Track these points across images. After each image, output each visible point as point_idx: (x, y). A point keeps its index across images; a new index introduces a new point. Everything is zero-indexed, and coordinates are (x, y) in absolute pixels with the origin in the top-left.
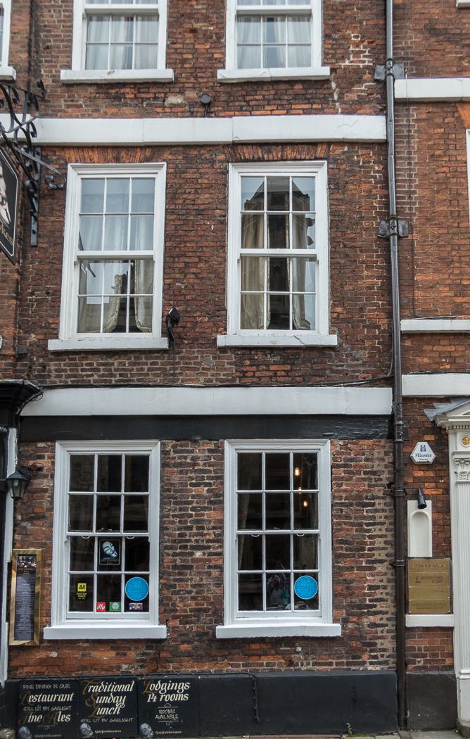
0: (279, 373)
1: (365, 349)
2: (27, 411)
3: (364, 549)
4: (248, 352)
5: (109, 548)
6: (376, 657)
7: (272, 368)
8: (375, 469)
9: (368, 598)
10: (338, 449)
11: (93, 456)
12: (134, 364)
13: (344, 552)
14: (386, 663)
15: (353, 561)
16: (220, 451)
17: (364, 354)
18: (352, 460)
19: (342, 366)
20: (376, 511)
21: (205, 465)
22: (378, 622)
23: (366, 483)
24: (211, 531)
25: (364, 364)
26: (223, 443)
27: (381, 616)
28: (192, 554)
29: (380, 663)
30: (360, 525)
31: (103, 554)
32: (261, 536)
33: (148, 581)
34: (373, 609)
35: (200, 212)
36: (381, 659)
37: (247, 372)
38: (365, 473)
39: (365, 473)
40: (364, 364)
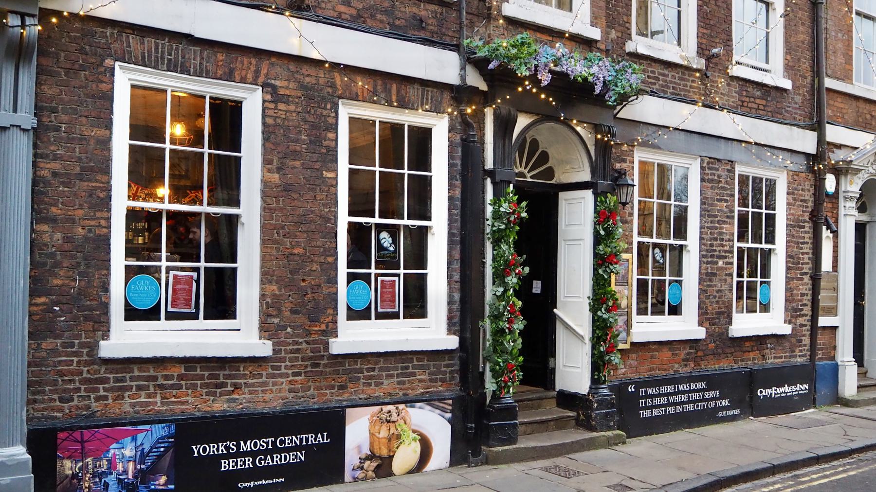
5: (386, 239)
6: (801, 351)
12: (683, 79)
22: (804, 323)
24: (727, 243)
28: (717, 263)
30: (798, 243)
31: (380, 247)
32: (160, 213)
33: (681, 286)
38: (802, 201)
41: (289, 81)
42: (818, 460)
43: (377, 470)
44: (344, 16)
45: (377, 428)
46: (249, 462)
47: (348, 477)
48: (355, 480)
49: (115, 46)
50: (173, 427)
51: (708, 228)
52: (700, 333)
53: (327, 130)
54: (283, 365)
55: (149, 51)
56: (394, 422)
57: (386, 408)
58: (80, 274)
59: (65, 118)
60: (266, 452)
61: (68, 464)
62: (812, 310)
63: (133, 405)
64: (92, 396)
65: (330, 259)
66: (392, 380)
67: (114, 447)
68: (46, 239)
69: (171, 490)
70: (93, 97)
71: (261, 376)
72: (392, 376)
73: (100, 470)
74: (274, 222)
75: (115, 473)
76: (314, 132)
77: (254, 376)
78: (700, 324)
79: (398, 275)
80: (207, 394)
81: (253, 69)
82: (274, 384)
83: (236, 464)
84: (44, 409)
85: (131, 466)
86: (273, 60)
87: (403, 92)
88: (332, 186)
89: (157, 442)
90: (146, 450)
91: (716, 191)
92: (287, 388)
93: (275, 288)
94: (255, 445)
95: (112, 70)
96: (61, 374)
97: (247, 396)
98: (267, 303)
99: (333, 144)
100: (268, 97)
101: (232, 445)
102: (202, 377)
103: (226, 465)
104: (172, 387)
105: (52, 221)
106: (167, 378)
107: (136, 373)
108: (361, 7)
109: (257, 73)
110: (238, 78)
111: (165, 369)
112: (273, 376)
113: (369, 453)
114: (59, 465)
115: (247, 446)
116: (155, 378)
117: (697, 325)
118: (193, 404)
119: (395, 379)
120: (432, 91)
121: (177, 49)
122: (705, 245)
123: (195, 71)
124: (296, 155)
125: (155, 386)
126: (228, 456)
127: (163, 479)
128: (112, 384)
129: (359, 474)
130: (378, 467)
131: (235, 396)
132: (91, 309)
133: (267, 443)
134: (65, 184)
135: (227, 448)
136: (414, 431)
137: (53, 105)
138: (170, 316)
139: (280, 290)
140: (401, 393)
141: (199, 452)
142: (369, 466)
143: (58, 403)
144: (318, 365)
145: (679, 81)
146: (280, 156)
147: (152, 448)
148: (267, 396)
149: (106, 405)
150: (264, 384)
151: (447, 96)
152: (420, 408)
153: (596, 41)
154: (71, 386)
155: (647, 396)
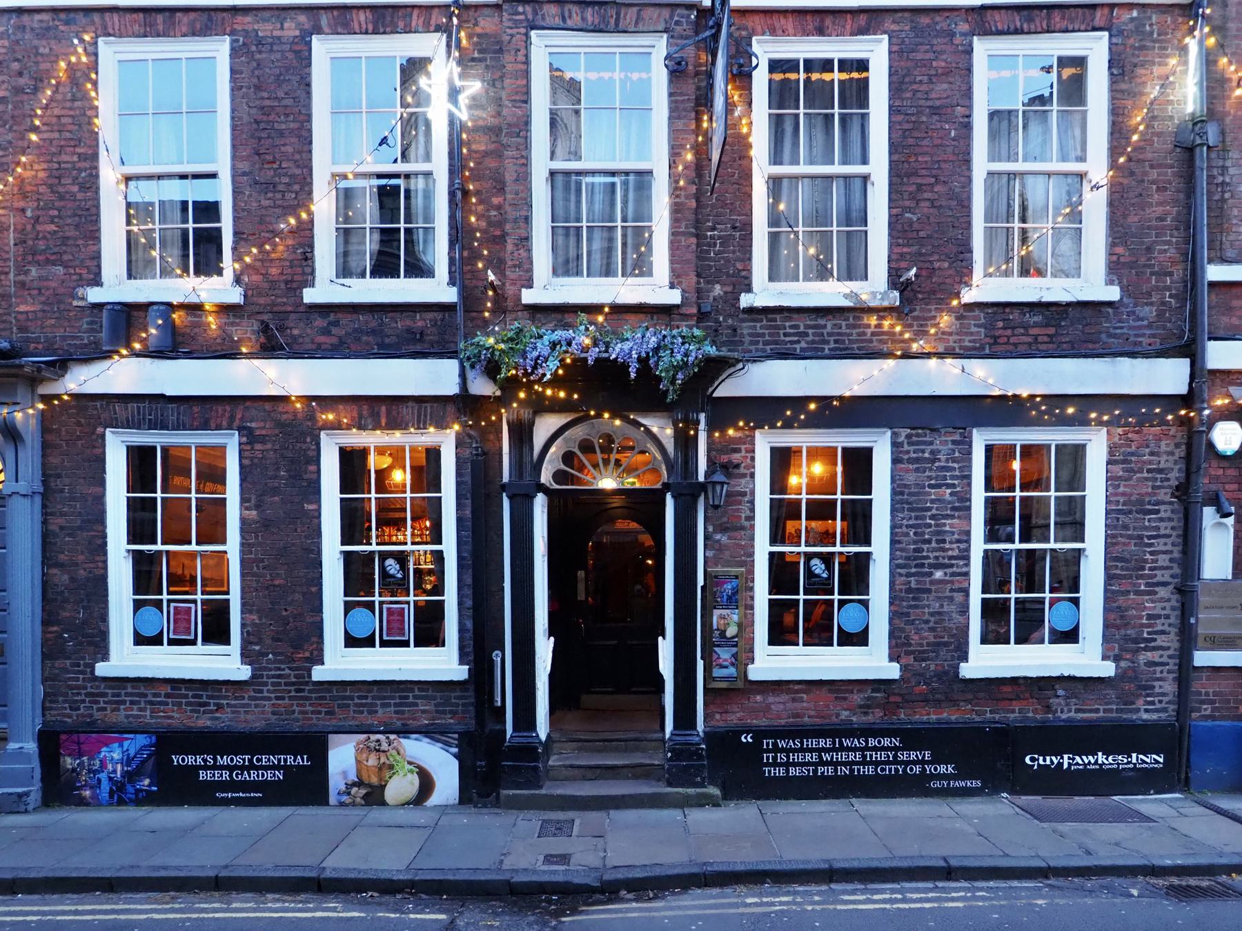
0: (1040, 339)
1: (1152, 304)
2: (726, 389)
3: (1143, 568)
4: (1000, 310)
5: (818, 567)
7: (1032, 331)
8: (1162, 466)
9: (1146, 630)
10: (1116, 439)
11: (836, 448)
13: (1118, 572)
14: (1164, 710)
15: (1131, 583)
16: (966, 445)
17: (1149, 312)
18: (1132, 454)
19: (1122, 328)
20: (1161, 520)
21: (947, 460)
22: (1157, 659)
23: (1150, 484)
24: (955, 546)
25: (1149, 326)
26: (971, 433)
27: (1161, 652)
28: (931, 574)
29: (1157, 711)
30: (1140, 537)
31: (384, 574)
34: (1153, 644)
35: (935, 111)
36: (1158, 706)
37: (999, 337)
38: (1149, 471)
39: (1149, 471)
40: (1149, 326)
41: (265, 421)
42: (949, 873)
43: (365, 797)
44: (1040, 339)
45: (364, 756)
46: (226, 775)
47: (333, 800)
48: (342, 804)
49: (104, 416)
50: (154, 738)
51: (907, 526)
52: (892, 671)
53: (308, 462)
54: (265, 689)
55: (133, 416)
56: (384, 751)
57: (374, 737)
58: (83, 607)
59: (67, 481)
60: (242, 768)
61: (69, 760)
62: (1181, 641)
63: (127, 717)
64: (95, 707)
65: (314, 589)
66: (388, 710)
67: (104, 751)
68: (56, 580)
69: (154, 791)
70: (89, 461)
71: (243, 698)
72: (389, 705)
73: (94, 768)
74: (253, 556)
75: (106, 771)
76: (293, 467)
77: (236, 698)
78: (892, 658)
79: (195, 602)
80: (191, 711)
81: (227, 415)
82: (256, 706)
83: (214, 775)
84: (59, 715)
85: (119, 767)
86: (248, 404)
87: (394, 413)
88: (314, 517)
89: (141, 749)
90: (132, 755)
91: (927, 473)
92: (270, 710)
93: (255, 617)
94: (232, 760)
95: (103, 436)
96: (71, 688)
97: (230, 715)
98: (248, 632)
99: (314, 476)
100: (244, 439)
101: (209, 758)
102: (186, 696)
103: (203, 775)
104: (160, 703)
105: (60, 565)
106: (155, 695)
107: (130, 690)
108: (344, 332)
109: (232, 418)
110: (213, 425)
111: (153, 688)
112: (256, 699)
113: (356, 780)
114: (62, 760)
115: (224, 760)
116: (145, 695)
117: (887, 659)
118: (179, 719)
119: (392, 709)
120: (431, 407)
121: (157, 408)
122: (902, 550)
123: (173, 426)
124: (275, 491)
125: (145, 702)
126: (206, 768)
127: (147, 782)
128: (110, 698)
129: (345, 798)
130: (366, 795)
131: (217, 715)
132: (93, 636)
133: (244, 760)
134: (69, 535)
135: (205, 760)
136: (410, 763)
137: (59, 471)
138: (172, 642)
139: (260, 619)
140: (399, 723)
141: (178, 761)
142: (357, 792)
143: (68, 711)
144: (302, 691)
145: (848, 331)
146: (258, 493)
147: (136, 754)
148: (249, 717)
149: (106, 715)
150: (248, 705)
151: (451, 409)
152: (416, 739)
153: (677, 306)
154: (79, 698)
155: (776, 749)
